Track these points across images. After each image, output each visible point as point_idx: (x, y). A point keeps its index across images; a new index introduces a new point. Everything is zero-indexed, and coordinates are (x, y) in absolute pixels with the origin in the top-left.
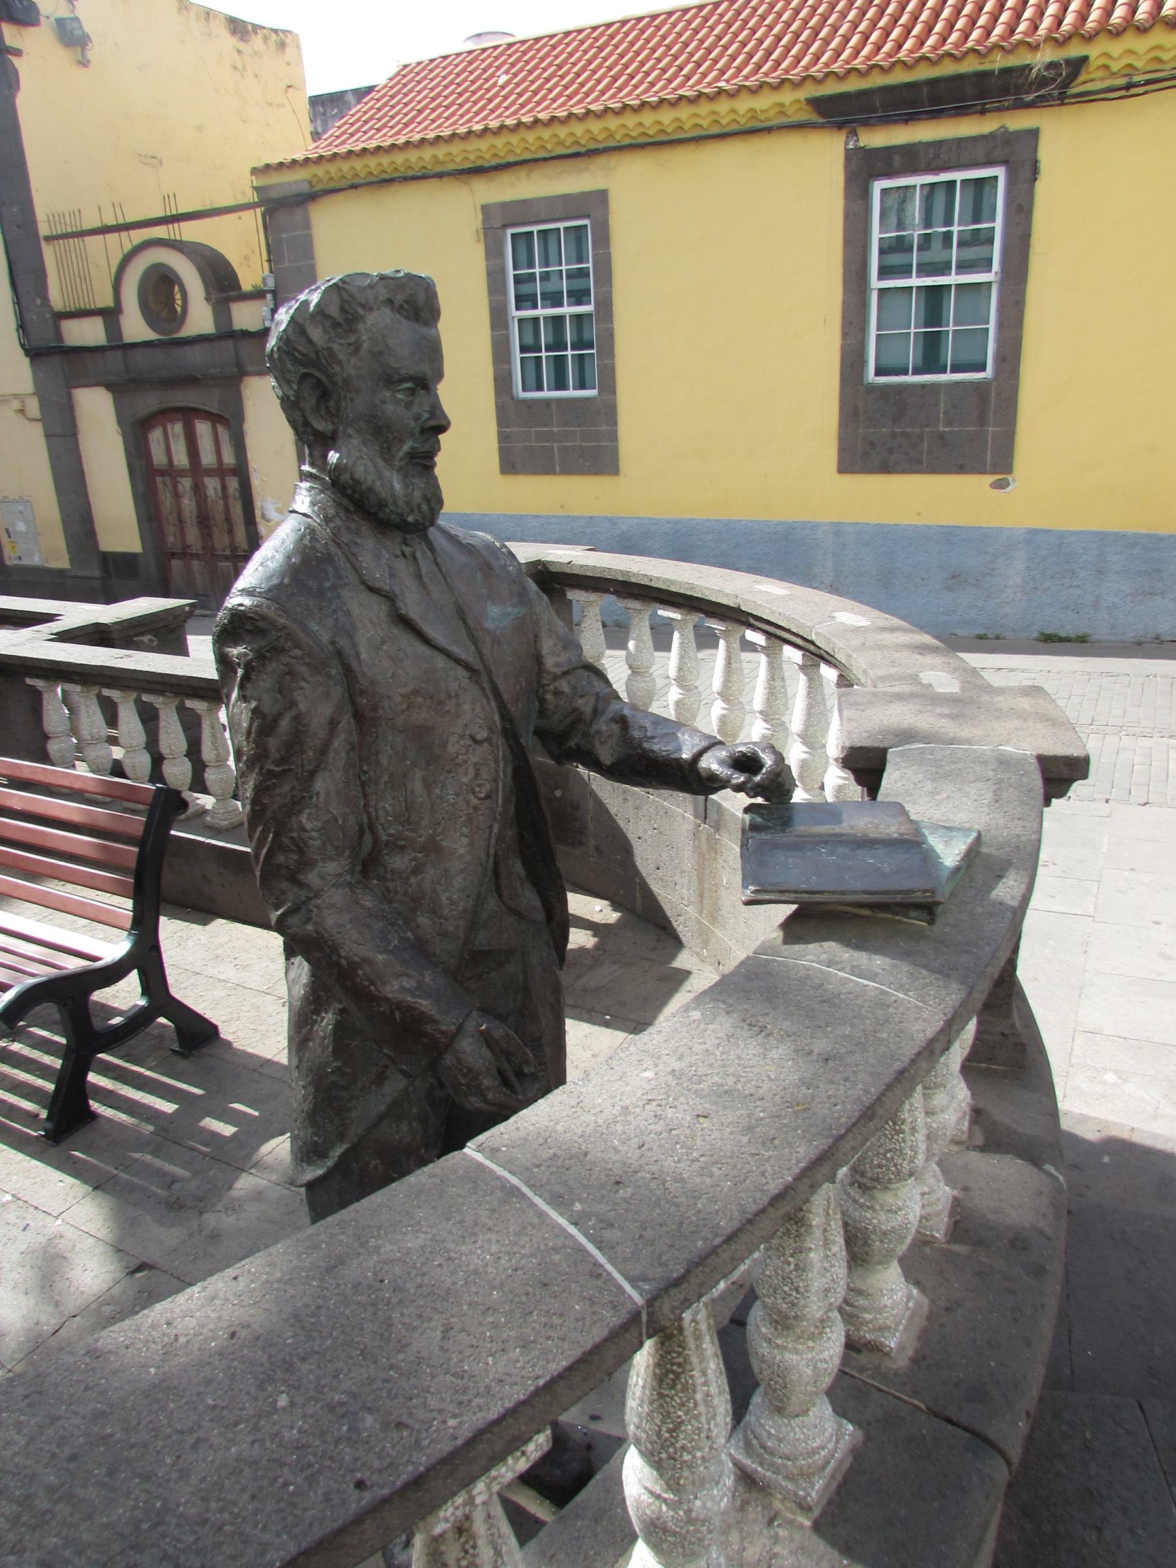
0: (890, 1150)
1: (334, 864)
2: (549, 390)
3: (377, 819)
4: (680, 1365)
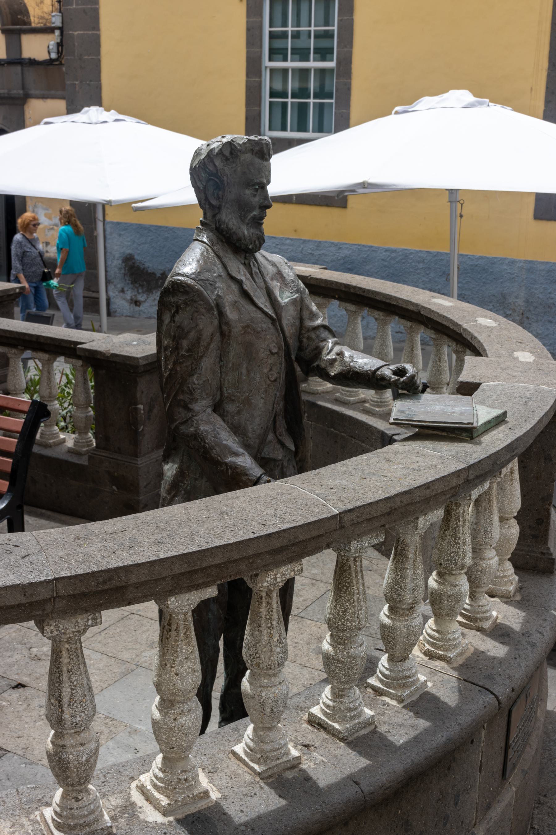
0: (453, 552)
1: (205, 402)
2: (291, 131)
3: (224, 384)
4: (348, 583)
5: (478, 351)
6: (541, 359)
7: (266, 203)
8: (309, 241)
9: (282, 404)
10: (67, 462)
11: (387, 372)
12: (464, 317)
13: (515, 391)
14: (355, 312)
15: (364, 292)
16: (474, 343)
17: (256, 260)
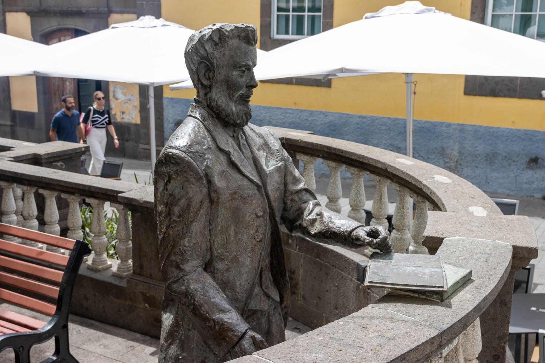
1: (195, 262)
2: (292, 34)
3: (214, 245)
5: (437, 205)
6: (493, 214)
7: (252, 85)
8: (305, 110)
9: (268, 260)
10: (111, 284)
11: (362, 233)
12: (424, 174)
13: (475, 247)
14: (336, 168)
15: (342, 152)
16: (433, 197)
17: (244, 133)
